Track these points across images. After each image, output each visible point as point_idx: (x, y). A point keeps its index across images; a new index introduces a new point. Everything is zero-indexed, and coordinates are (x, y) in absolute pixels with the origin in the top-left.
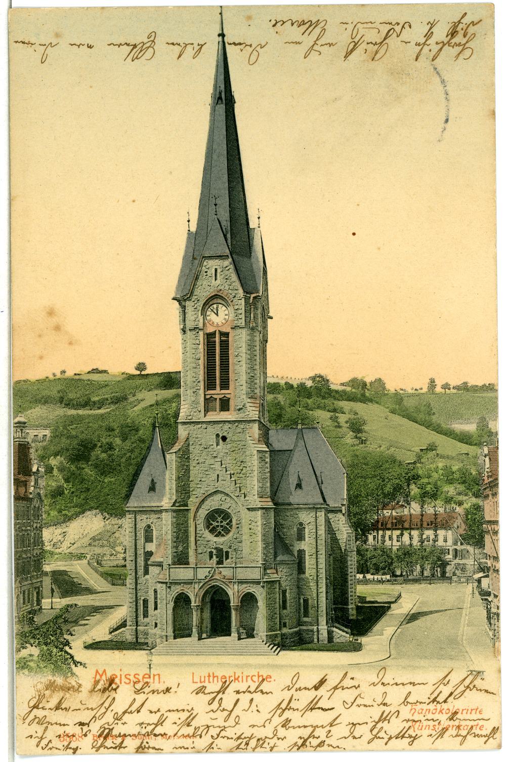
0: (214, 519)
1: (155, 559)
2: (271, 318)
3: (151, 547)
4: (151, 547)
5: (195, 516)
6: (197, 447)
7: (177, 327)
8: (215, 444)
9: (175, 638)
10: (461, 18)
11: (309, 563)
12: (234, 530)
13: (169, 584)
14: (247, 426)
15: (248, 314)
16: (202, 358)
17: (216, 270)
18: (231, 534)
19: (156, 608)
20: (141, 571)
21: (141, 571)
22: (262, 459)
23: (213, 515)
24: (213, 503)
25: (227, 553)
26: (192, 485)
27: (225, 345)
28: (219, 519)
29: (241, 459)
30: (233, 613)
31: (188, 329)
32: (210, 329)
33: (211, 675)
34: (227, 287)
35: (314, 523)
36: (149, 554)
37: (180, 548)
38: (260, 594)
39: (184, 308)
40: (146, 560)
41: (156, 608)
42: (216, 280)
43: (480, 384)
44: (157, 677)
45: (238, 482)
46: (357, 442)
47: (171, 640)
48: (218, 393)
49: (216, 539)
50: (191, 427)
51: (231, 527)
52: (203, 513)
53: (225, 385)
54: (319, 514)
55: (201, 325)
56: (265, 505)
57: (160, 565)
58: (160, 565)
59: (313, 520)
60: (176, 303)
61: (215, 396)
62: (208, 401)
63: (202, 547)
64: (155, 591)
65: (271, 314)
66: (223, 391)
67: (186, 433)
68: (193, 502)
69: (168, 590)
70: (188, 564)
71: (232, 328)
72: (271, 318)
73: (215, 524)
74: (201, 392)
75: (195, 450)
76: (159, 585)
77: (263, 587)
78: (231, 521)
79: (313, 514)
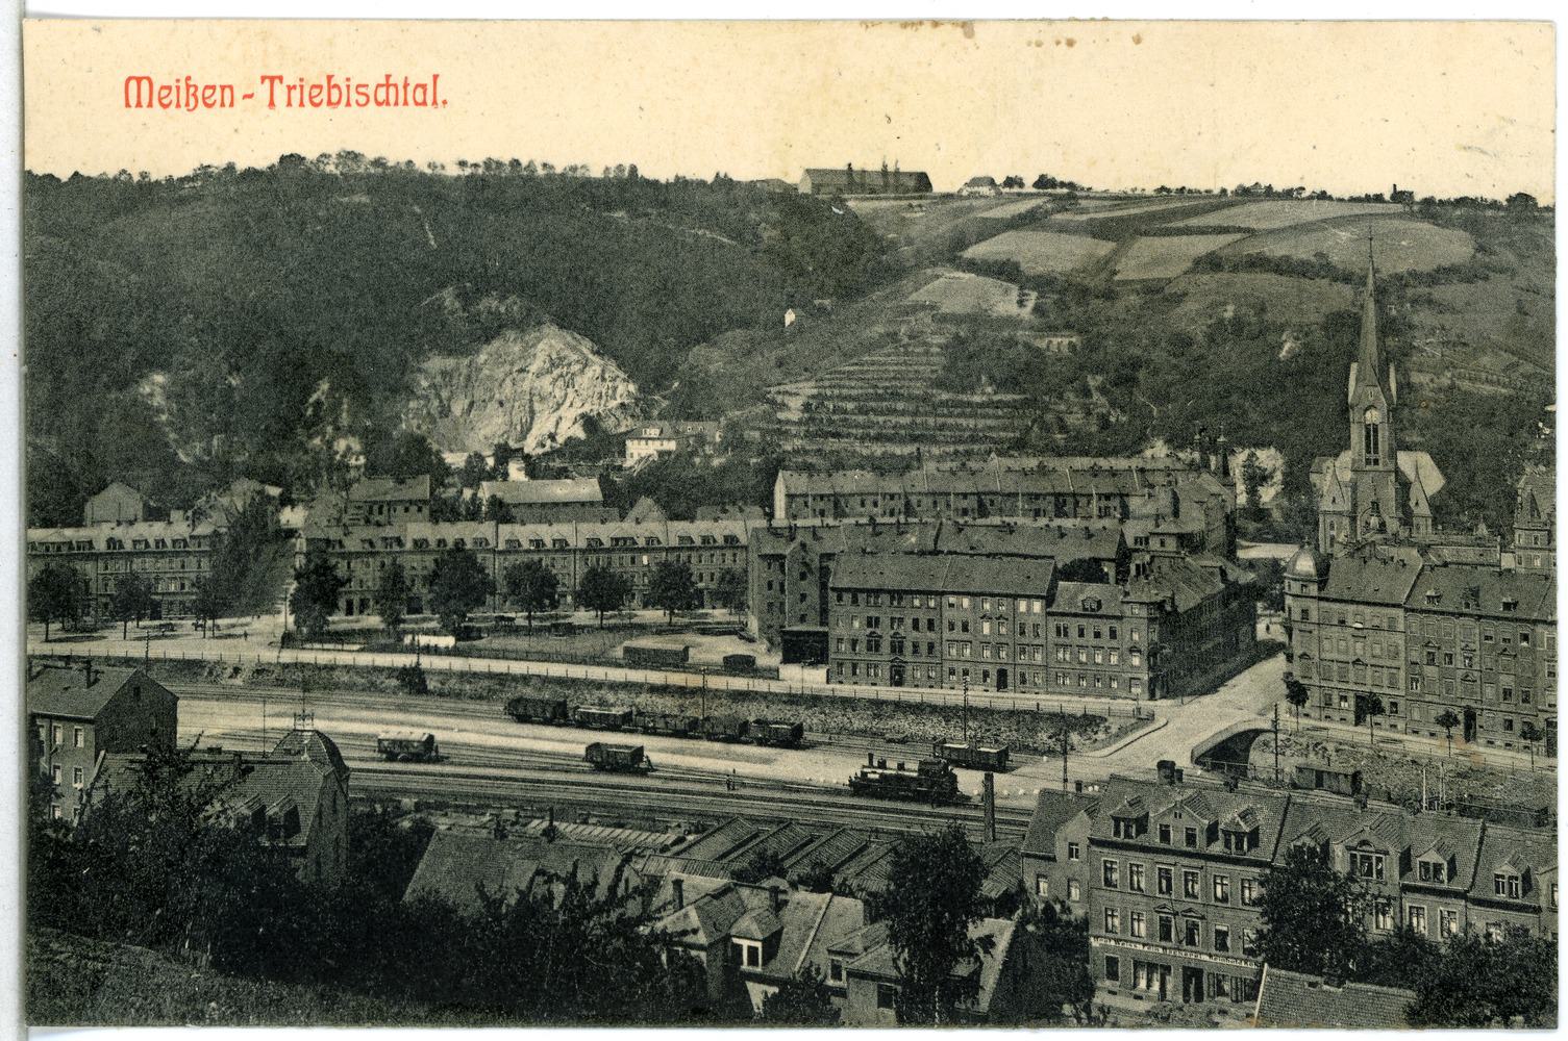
53: (1376, 452)
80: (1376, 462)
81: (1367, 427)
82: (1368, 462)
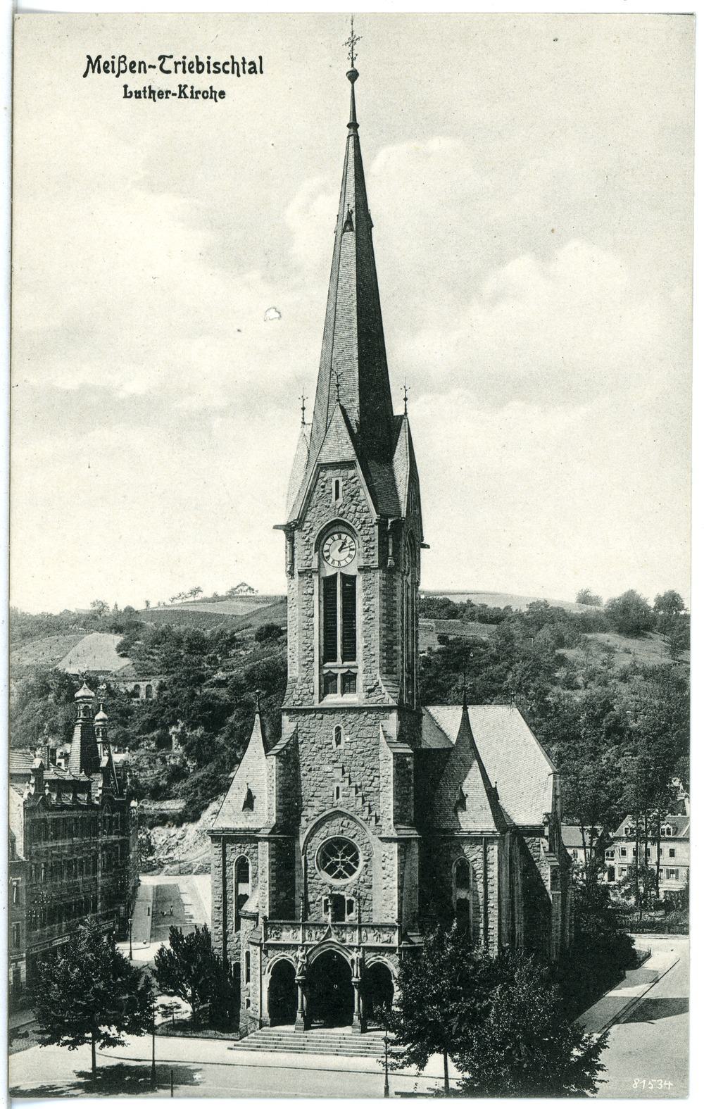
33: (147, 90)
44: (142, 65)
53: (350, 654)
80: (349, 681)
81: (329, 583)
82: (327, 684)
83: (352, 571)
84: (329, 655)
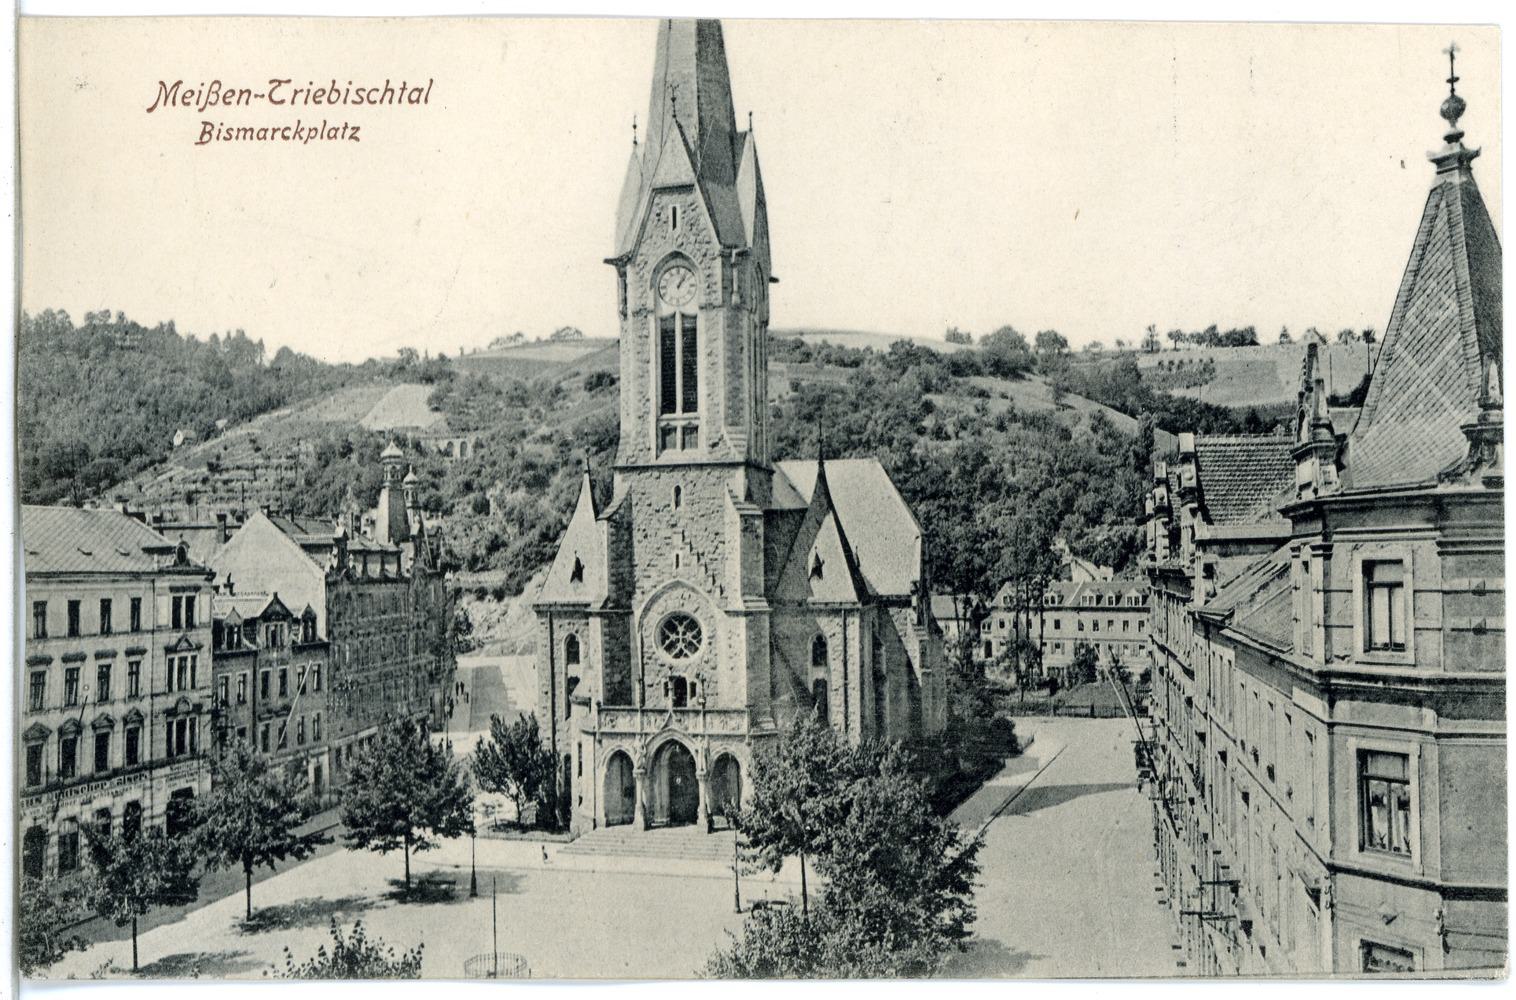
0: (674, 629)
1: (580, 691)
2: (774, 280)
3: (574, 670)
4: (574, 670)
5: (641, 625)
6: (645, 508)
7: (614, 306)
8: (673, 505)
9: (608, 824)
10: (124, 972)
11: (835, 701)
12: (703, 647)
13: (598, 737)
14: (726, 472)
15: (727, 283)
16: (653, 360)
17: (674, 210)
18: (698, 654)
19: (580, 774)
20: (561, 711)
21: (561, 711)
22: (747, 529)
23: (671, 624)
24: (670, 604)
25: (693, 685)
26: (638, 572)
27: (690, 335)
28: (681, 629)
29: (716, 529)
30: (702, 786)
31: (629, 312)
32: (666, 310)
34: (692, 239)
35: (841, 636)
36: (573, 682)
37: (617, 678)
38: (743, 753)
39: (623, 275)
40: (569, 692)
41: (580, 774)
42: (674, 226)
43: (357, 360)
45: (710, 567)
46: (783, 435)
47: (601, 829)
48: (679, 418)
49: (675, 662)
50: (634, 476)
51: (699, 642)
52: (655, 618)
53: (690, 405)
54: (850, 620)
55: (650, 305)
56: (753, 606)
57: (586, 703)
58: (586, 703)
59: (839, 630)
60: (612, 269)
61: (673, 423)
62: (665, 433)
63: (653, 675)
64: (580, 746)
65: (774, 274)
66: (687, 415)
67: (626, 485)
68: (638, 605)
69: (597, 746)
70: (630, 703)
71: (701, 308)
72: (774, 280)
73: (673, 637)
74: (652, 418)
75: (639, 518)
76: (584, 736)
77: (749, 744)
78: (699, 633)
79: (839, 620)
83: (691, 309)
84: (668, 405)
